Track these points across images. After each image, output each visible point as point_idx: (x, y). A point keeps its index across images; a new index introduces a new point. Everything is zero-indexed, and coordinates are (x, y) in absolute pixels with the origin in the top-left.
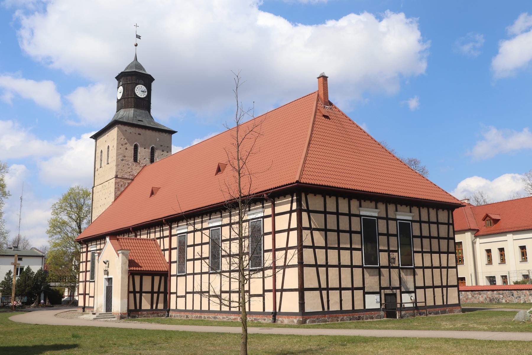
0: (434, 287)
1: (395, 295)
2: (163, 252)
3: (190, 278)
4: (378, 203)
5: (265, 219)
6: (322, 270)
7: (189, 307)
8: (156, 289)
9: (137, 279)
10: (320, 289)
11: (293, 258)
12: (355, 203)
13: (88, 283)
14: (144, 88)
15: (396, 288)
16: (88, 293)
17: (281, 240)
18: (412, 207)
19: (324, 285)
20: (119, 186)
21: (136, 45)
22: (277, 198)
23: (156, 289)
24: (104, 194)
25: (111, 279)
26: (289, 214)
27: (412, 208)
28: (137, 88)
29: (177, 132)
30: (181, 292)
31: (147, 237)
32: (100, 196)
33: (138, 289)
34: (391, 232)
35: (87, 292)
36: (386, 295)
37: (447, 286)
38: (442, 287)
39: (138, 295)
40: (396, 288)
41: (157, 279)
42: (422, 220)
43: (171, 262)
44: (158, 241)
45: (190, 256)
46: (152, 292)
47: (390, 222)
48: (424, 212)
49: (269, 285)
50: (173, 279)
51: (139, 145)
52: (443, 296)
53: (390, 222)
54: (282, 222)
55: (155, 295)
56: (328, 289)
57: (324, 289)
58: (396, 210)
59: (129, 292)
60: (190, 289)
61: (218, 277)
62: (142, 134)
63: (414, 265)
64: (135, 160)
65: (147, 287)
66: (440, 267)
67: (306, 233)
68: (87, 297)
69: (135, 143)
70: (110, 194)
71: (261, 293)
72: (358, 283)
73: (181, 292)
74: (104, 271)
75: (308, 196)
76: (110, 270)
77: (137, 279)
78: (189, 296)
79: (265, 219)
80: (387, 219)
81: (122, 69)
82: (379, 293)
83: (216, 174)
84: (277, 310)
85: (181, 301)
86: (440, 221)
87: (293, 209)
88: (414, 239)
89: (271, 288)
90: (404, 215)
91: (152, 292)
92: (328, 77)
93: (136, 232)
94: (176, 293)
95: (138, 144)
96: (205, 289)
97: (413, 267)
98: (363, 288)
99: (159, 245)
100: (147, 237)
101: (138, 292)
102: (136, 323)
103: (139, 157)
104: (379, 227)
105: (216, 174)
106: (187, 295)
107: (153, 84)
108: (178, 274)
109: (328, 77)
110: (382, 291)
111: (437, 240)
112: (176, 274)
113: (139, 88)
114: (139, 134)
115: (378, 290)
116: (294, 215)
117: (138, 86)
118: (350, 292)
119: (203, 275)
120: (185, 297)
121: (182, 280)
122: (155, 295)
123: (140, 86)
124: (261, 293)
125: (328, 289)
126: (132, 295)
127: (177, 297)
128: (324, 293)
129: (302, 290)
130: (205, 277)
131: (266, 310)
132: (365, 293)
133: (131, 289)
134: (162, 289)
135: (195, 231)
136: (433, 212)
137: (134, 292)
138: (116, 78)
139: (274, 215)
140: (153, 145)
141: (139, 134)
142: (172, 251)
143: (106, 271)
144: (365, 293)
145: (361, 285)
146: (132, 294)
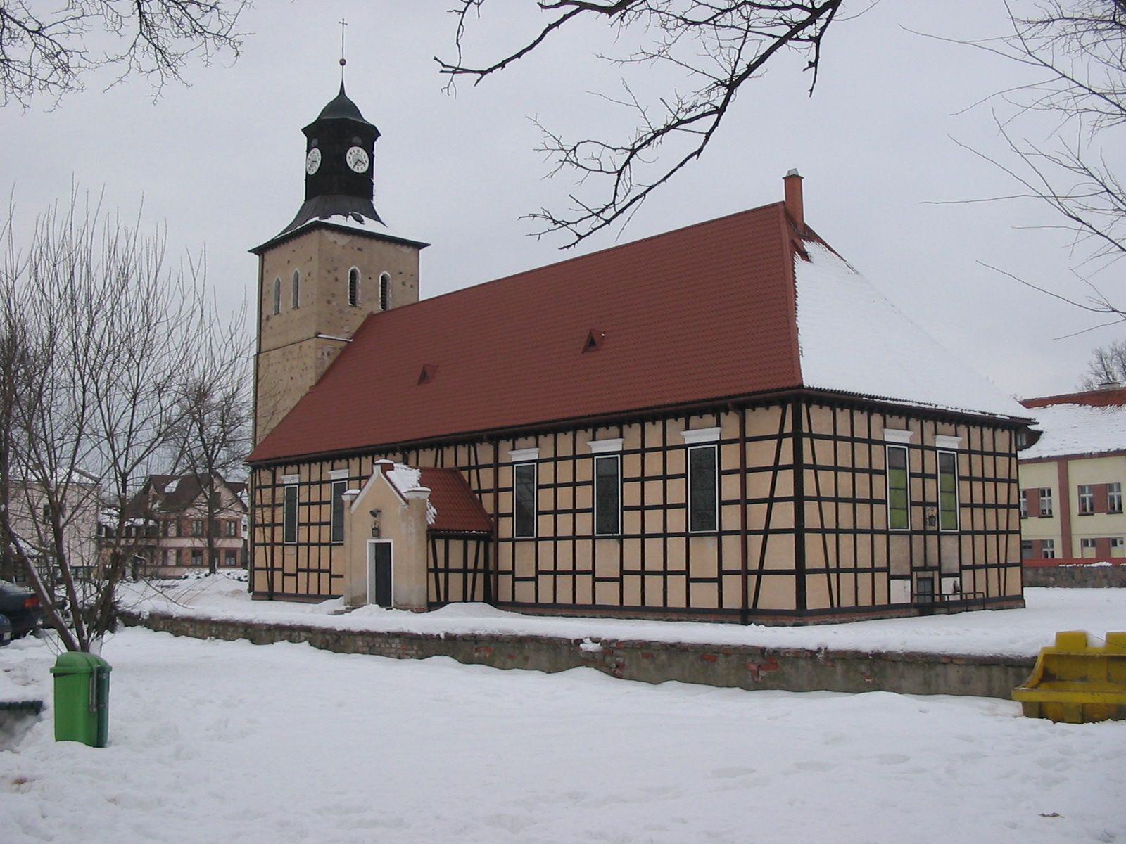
0: (308, 570)
1: (932, 580)
2: (477, 495)
3: (1002, 537)
4: (872, 414)
5: (722, 446)
6: (831, 538)
7: (302, 591)
8: (470, 565)
9: (440, 544)
10: (827, 571)
11: (784, 515)
12: (877, 419)
13: (278, 549)
14: (362, 154)
15: (933, 569)
16: (328, 568)
17: (759, 485)
18: (959, 426)
19: (833, 565)
20: (323, 354)
21: (343, 63)
22: (749, 410)
23: (470, 565)
24: (289, 369)
25: (387, 546)
26: (776, 441)
27: (958, 428)
28: (358, 151)
29: (429, 245)
30: (290, 568)
31: (436, 464)
32: (278, 372)
33: (441, 565)
34: (927, 471)
35: (278, 564)
36: (918, 579)
37: (1006, 565)
38: (998, 566)
39: (442, 576)
40: (933, 569)
41: (472, 545)
42: (1069, 462)
43: (498, 515)
44: (465, 474)
45: (303, 517)
46: (465, 571)
47: (926, 452)
48: (843, 416)
49: (732, 560)
50: (505, 548)
51: (359, 271)
52: (1000, 589)
53: (926, 452)
54: (761, 454)
55: (470, 576)
56: (838, 571)
57: (441, 570)
58: (936, 433)
59: (429, 570)
60: (303, 565)
61: (711, 543)
62: (356, 249)
63: (622, 532)
64: (353, 300)
65: (456, 561)
66: (997, 532)
67: (808, 475)
68: (278, 575)
69: (351, 269)
70: (303, 370)
71: (295, 572)
72: (584, 563)
73: (290, 568)
74: (373, 529)
75: (810, 409)
76: (383, 528)
77: (440, 544)
78: (302, 576)
79: (722, 446)
80: (922, 447)
81: (312, 118)
82: (909, 577)
83: (585, 351)
84: (750, 606)
85: (290, 582)
86: (998, 450)
87: (784, 432)
88: (960, 482)
89: (737, 566)
90: (947, 441)
91: (465, 571)
92: (803, 178)
93: (406, 453)
94: (282, 569)
95: (357, 269)
96: (935, 563)
97: (958, 531)
98: (887, 570)
99: (467, 481)
100: (436, 464)
101: (753, 572)
102: (520, 631)
103: (359, 299)
104: (911, 462)
105: (585, 351)
106: (624, 576)
107: (378, 145)
108: (285, 543)
109: (803, 178)
110: (914, 573)
111: (920, 480)
112: (281, 542)
113: (353, 154)
114: (360, 249)
115: (908, 573)
116: (788, 444)
117: (351, 150)
118: (322, 541)
119: (307, 521)
120: (296, 575)
121: (290, 551)
122: (470, 576)
123: (355, 148)
124: (295, 572)
125: (838, 571)
126: (432, 575)
127: (284, 575)
128: (833, 576)
129: (800, 572)
130: (325, 550)
131: (578, 602)
132: (890, 577)
133: (432, 566)
134: (481, 565)
135: (310, 484)
136: (860, 418)
137: (436, 570)
138: (305, 130)
139: (743, 440)
140: (385, 272)
141: (360, 249)
142: (501, 494)
143: (375, 529)
144: (890, 577)
145: (884, 565)
146: (433, 574)
